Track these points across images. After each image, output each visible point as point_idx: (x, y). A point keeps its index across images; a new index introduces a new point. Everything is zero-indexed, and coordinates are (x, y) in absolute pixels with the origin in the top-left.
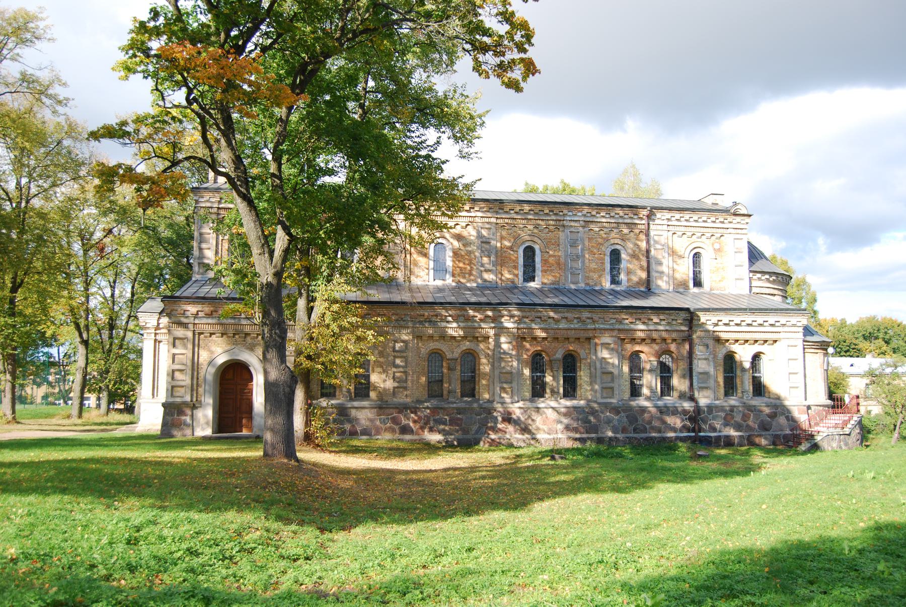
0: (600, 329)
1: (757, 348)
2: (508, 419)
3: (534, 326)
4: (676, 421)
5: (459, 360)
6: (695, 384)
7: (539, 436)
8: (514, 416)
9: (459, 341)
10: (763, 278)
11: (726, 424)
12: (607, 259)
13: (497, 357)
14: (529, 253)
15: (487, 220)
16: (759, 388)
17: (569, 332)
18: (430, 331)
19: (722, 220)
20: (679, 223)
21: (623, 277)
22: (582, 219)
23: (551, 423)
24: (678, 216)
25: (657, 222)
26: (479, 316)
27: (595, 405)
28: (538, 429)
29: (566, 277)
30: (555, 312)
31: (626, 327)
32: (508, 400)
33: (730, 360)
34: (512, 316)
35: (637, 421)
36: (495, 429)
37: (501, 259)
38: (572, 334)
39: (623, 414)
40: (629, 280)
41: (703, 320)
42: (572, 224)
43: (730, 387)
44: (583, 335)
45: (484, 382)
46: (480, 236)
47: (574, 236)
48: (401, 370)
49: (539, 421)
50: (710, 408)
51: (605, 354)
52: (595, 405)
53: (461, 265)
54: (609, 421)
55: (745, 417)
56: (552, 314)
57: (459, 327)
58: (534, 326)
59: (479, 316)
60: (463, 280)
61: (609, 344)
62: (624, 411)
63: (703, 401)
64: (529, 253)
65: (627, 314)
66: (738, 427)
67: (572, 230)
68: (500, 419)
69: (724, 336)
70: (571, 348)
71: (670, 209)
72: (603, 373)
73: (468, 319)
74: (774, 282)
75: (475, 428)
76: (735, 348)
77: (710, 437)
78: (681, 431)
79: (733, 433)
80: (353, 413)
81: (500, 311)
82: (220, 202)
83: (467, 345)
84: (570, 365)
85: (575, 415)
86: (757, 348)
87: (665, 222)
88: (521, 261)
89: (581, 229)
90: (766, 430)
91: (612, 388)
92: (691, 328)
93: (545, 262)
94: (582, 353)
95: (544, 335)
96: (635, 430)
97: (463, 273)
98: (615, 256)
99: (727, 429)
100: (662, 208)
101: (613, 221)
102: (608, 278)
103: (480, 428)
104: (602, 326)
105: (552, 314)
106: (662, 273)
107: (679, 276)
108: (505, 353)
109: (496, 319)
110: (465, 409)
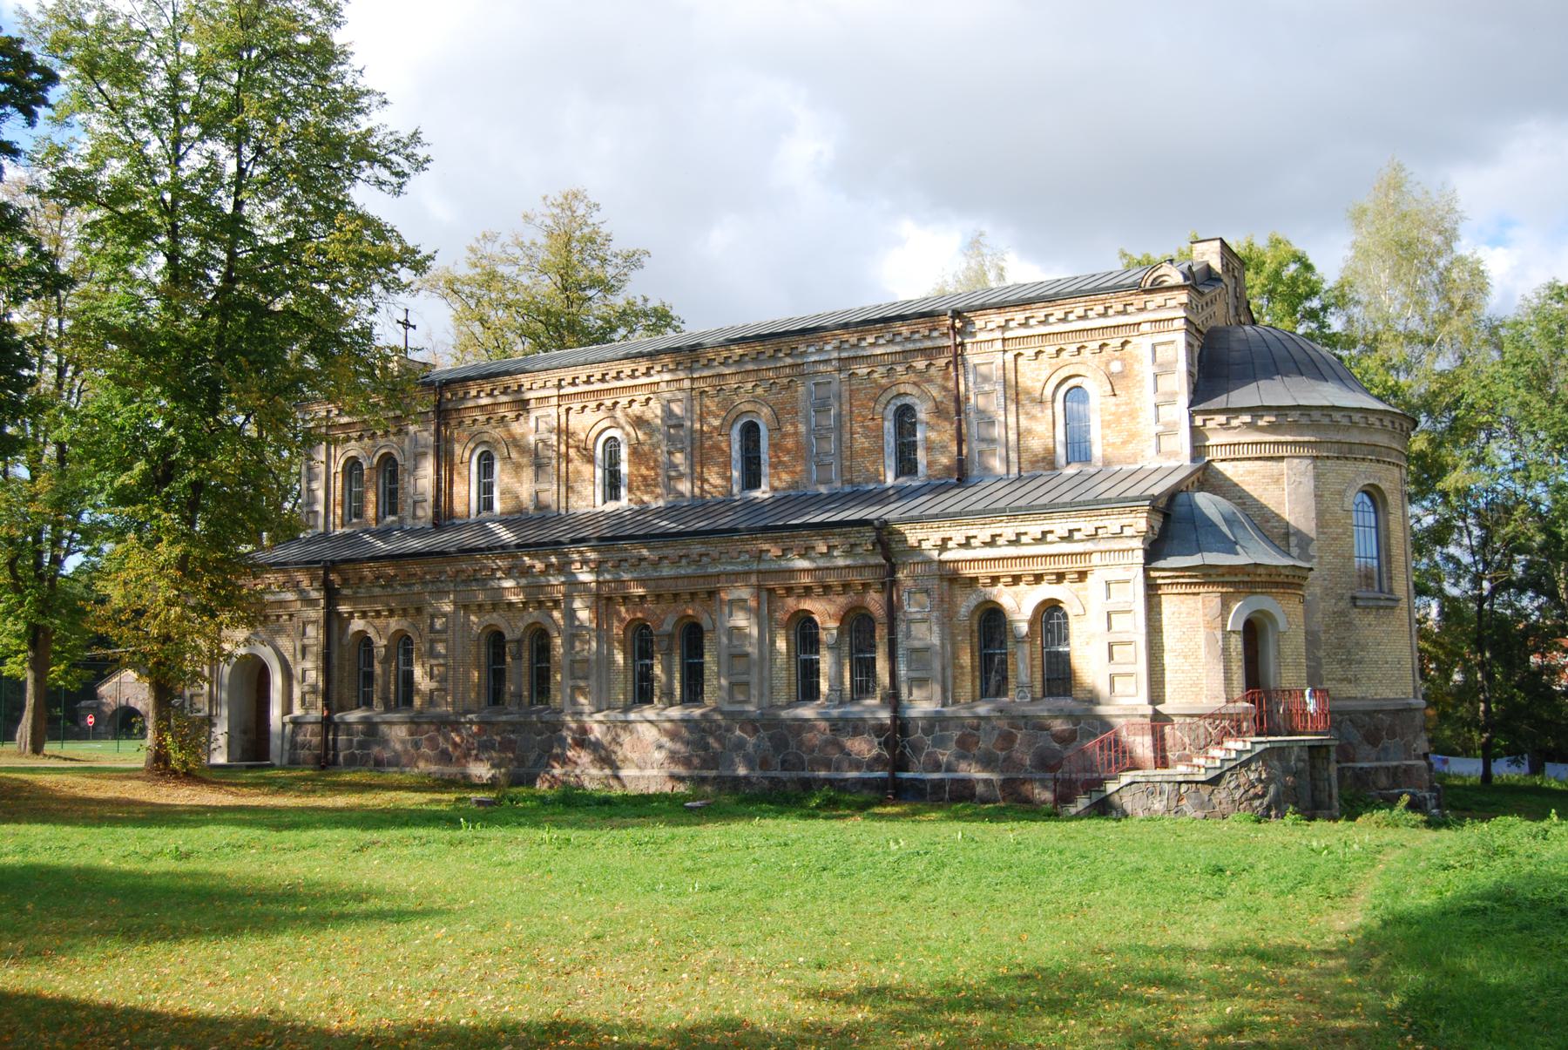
0: (728, 574)
1: (1046, 591)
2: (582, 741)
3: (626, 577)
4: (864, 747)
5: (527, 642)
6: (903, 671)
7: (623, 773)
8: (592, 737)
9: (520, 610)
10: (1235, 423)
11: (962, 757)
12: (889, 426)
13: (574, 632)
14: (751, 432)
15: (676, 385)
16: (1059, 676)
17: (680, 582)
18: (481, 597)
19: (1120, 308)
20: (606, 386)
21: (921, 457)
22: (835, 355)
23: (646, 751)
24: (1020, 317)
25: (981, 336)
26: (539, 566)
27: (718, 717)
28: (625, 760)
29: (809, 472)
30: (649, 549)
31: (774, 566)
32: (587, 709)
33: (992, 619)
34: (584, 562)
35: (786, 745)
36: (565, 761)
37: (701, 452)
38: (682, 586)
39: (762, 733)
40: (930, 465)
41: (912, 539)
42: (822, 368)
43: (992, 675)
44: (702, 586)
45: (559, 677)
46: (668, 413)
47: (822, 392)
48: (442, 661)
49: (626, 748)
50: (935, 722)
51: (740, 620)
52: (718, 717)
53: (644, 471)
54: (740, 745)
55: (1008, 739)
56: (645, 552)
57: (518, 586)
58: (626, 577)
59: (539, 566)
60: (646, 498)
61: (745, 601)
62: (766, 727)
63: (921, 705)
64: (751, 432)
65: (766, 540)
66: (987, 762)
67: (819, 379)
68: (569, 740)
69: (968, 572)
70: (690, 612)
71: (1000, 307)
72: (733, 656)
73: (527, 571)
74: (1272, 428)
75: (533, 756)
76: (1005, 597)
77: (922, 781)
78: (870, 768)
79: (977, 773)
80: (384, 728)
81: (566, 555)
82: (559, 387)
83: (533, 614)
84: (693, 638)
85: (684, 733)
86: (1046, 591)
87: (998, 334)
88: (736, 453)
89: (836, 374)
90: (1053, 769)
91: (747, 684)
92: (888, 559)
93: (775, 447)
94: (706, 622)
95: (640, 591)
96: (785, 765)
97: (648, 484)
98: (905, 418)
99: (963, 765)
100: (983, 307)
101: (898, 349)
102: (891, 462)
103: (540, 756)
104: (729, 568)
105: (645, 552)
106: (993, 441)
107: (1036, 444)
108: (582, 626)
109: (564, 568)
110: (520, 724)
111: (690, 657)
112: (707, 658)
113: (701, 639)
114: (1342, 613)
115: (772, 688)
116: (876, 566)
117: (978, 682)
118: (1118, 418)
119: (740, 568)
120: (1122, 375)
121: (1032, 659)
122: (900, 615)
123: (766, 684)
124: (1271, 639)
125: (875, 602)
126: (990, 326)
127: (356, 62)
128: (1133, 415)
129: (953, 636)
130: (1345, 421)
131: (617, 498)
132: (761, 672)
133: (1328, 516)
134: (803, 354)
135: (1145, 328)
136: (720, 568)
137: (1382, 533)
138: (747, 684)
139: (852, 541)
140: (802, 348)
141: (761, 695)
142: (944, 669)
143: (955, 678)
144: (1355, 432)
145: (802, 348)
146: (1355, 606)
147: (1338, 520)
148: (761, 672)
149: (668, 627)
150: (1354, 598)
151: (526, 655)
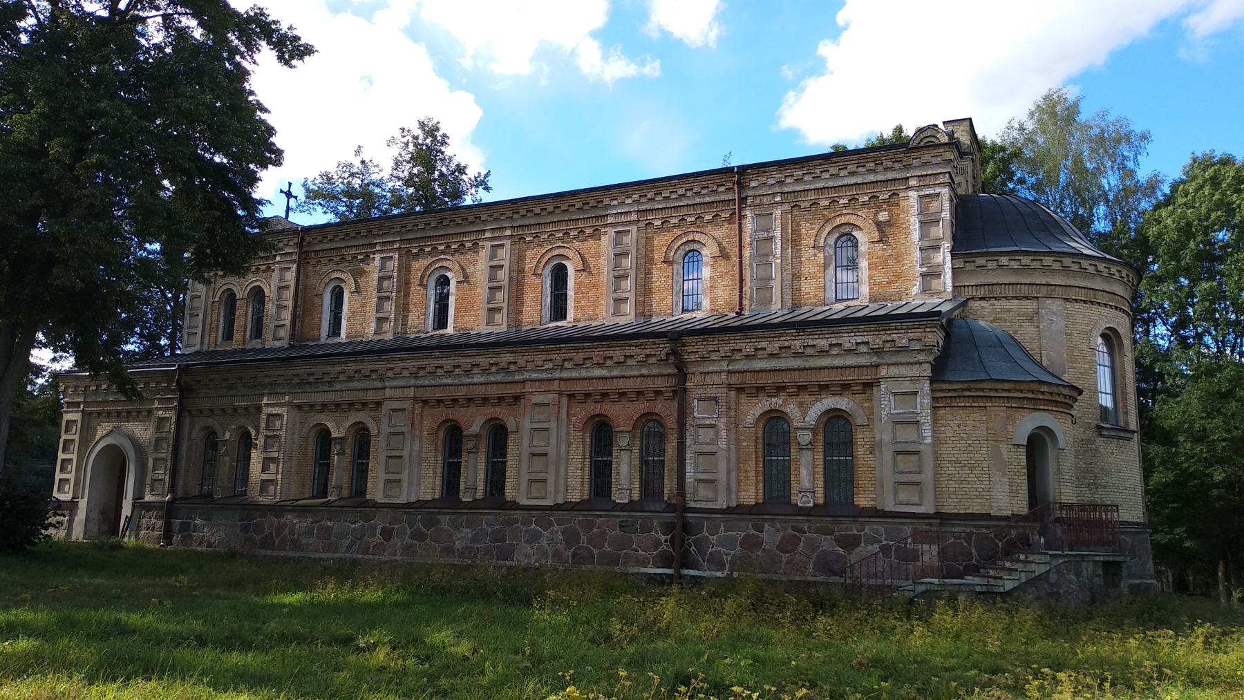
38: (493, 391)
44: (509, 390)
92: (680, 369)
104: (534, 375)
111: (494, 456)
112: (509, 457)
113: (506, 439)
114: (1089, 441)
115: (567, 486)
116: (669, 375)
117: (761, 487)
118: (885, 261)
119: (544, 376)
120: (889, 223)
121: (815, 466)
122: (689, 421)
123: (562, 482)
124: (1051, 454)
125: (666, 409)
126: (771, 181)
127: (332, 169)
128: (898, 259)
129: (738, 441)
130: (1091, 269)
131: (445, 326)
132: (557, 471)
133: (1076, 353)
134: (607, 207)
135: (913, 182)
136: (527, 375)
137: (1119, 373)
138: (544, 481)
139: (647, 352)
140: (607, 201)
141: (557, 492)
142: (729, 472)
143: (739, 481)
144: (1099, 279)
145: (607, 201)
146: (1101, 435)
147: (1085, 357)
148: (557, 471)
149: (475, 428)
150: (1099, 427)
151: (348, 451)
